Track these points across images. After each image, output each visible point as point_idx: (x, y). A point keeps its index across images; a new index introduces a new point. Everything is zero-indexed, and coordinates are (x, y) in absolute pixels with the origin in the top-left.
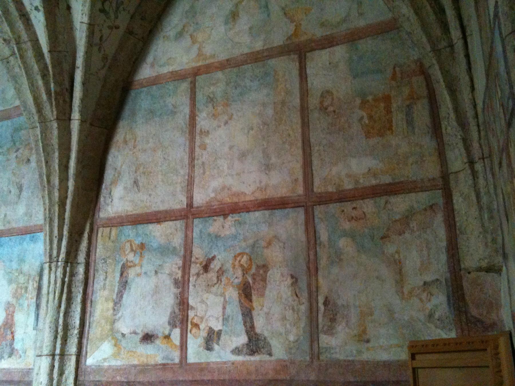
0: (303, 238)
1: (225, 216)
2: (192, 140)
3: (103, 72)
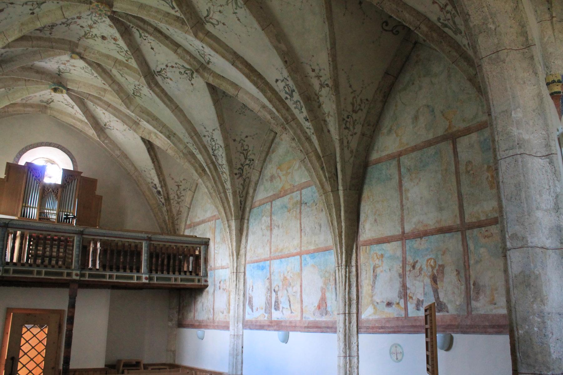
0: (462, 249)
1: (421, 238)
2: (401, 194)
3: (352, 159)
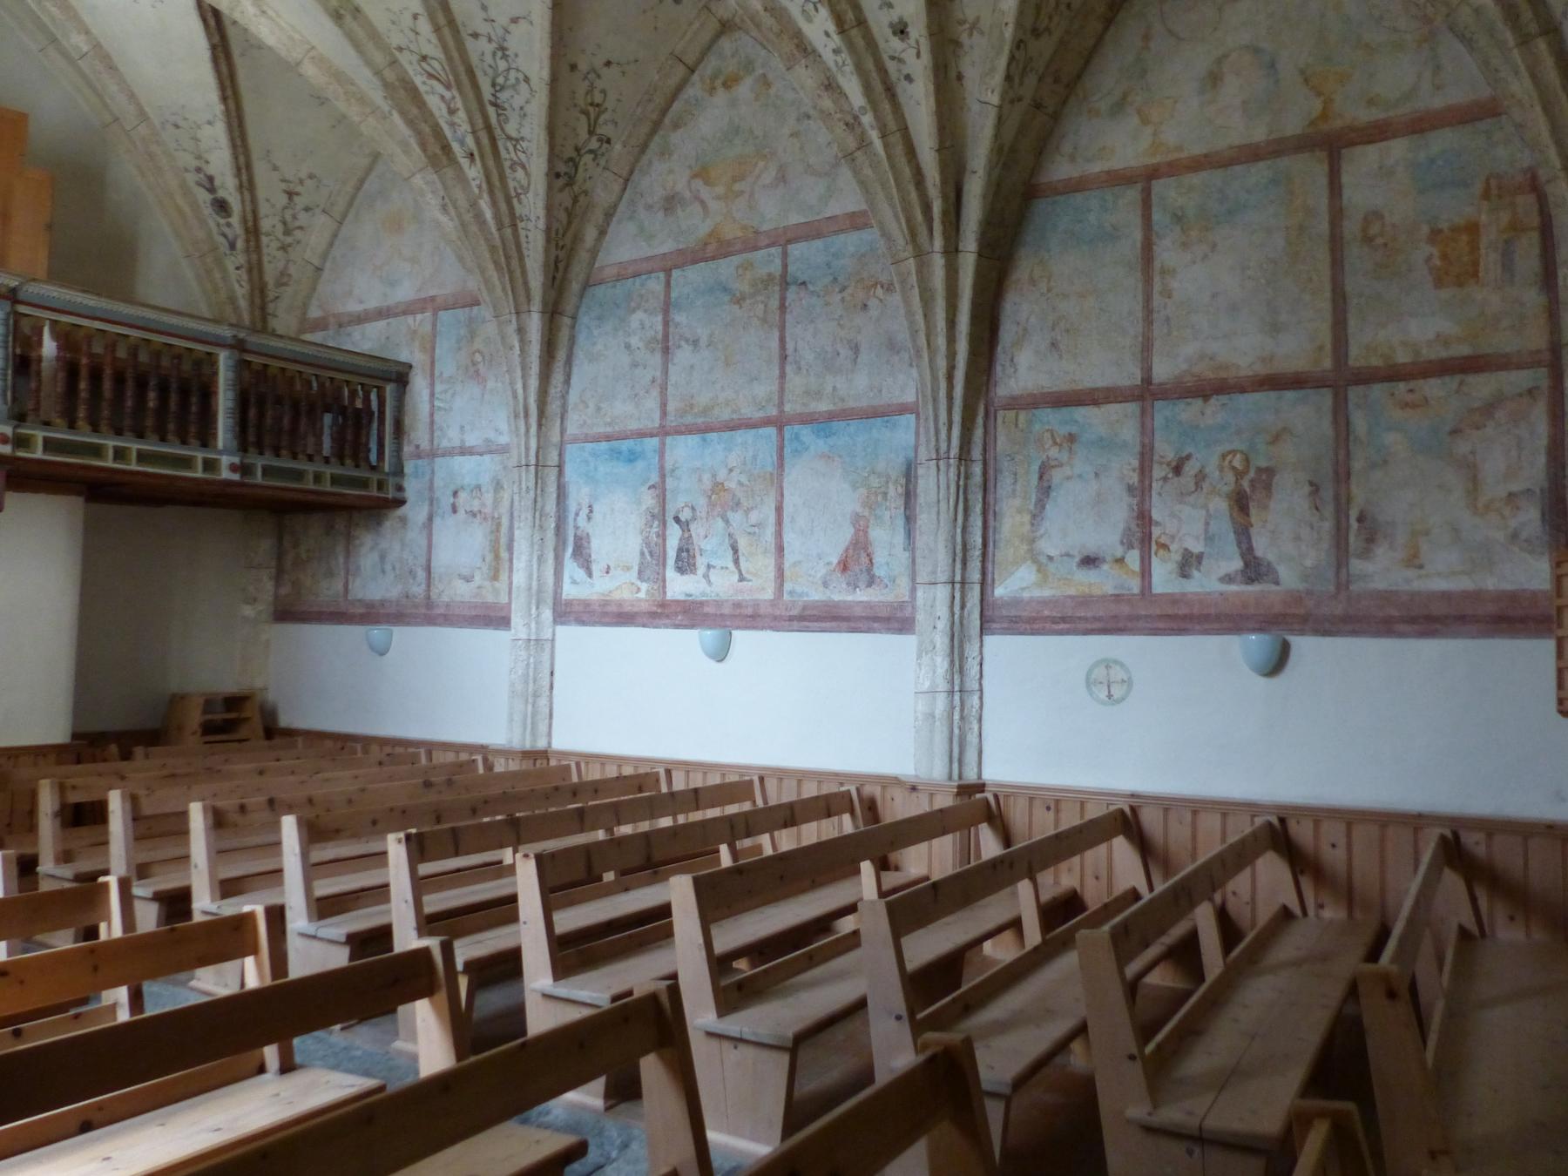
1: (1206, 398)
2: (1148, 281)
